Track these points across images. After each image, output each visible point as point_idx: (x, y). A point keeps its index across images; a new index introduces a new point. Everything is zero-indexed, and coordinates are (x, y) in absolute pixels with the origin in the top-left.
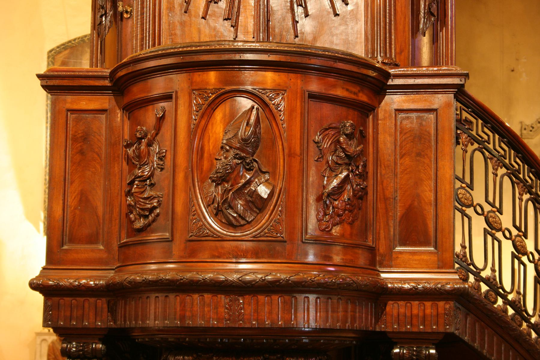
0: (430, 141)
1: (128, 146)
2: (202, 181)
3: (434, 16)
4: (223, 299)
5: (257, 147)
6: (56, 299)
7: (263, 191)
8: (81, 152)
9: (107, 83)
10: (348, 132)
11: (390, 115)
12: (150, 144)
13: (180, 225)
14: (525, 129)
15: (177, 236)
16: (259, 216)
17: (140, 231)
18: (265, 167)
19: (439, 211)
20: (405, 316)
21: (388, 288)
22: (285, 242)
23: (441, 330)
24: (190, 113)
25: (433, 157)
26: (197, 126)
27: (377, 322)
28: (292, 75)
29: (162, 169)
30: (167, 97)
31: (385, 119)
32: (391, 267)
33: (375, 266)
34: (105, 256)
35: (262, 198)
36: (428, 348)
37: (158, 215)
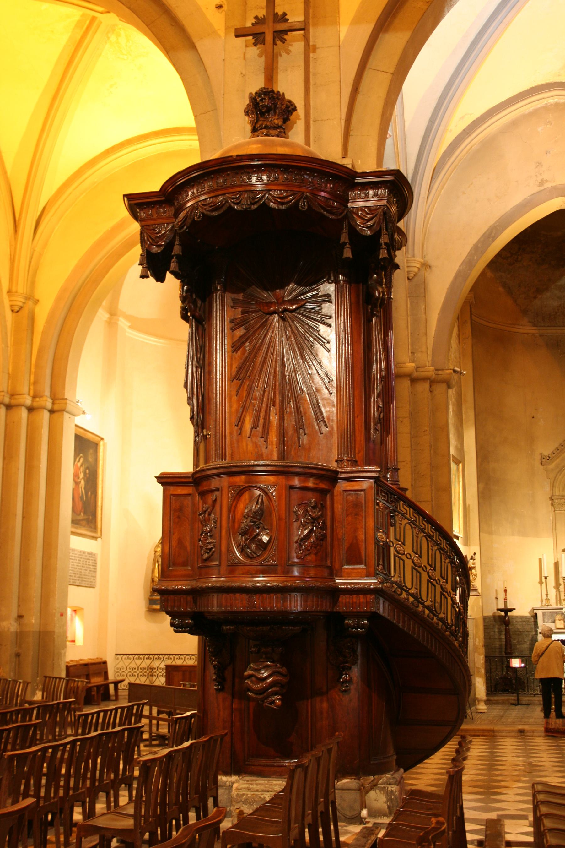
0: (362, 507)
1: (200, 514)
2: (234, 534)
3: (378, 431)
4: (245, 596)
5: (262, 516)
6: (166, 596)
7: (265, 539)
8: (179, 517)
9: (191, 480)
10: (312, 505)
11: (340, 493)
12: (210, 514)
13: (224, 557)
14: (544, 459)
15: (223, 563)
16: (264, 552)
17: (206, 560)
18: (267, 526)
19: (367, 545)
20: (349, 602)
21: (339, 588)
22: (277, 565)
23: (369, 610)
24: (228, 498)
25: (364, 515)
26: (232, 505)
27: (333, 607)
28: (280, 477)
29: (215, 528)
30: (217, 490)
31: (337, 495)
32: (341, 576)
33: (333, 576)
34: (191, 573)
35: (264, 543)
36: (363, 620)
37: (214, 552)
